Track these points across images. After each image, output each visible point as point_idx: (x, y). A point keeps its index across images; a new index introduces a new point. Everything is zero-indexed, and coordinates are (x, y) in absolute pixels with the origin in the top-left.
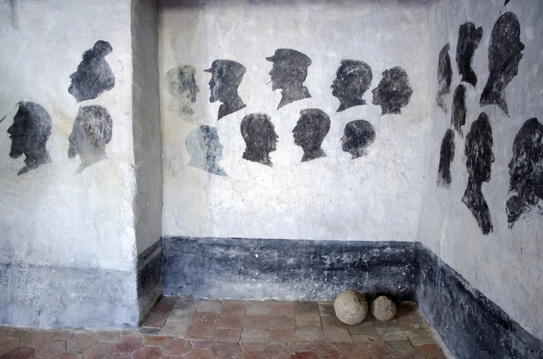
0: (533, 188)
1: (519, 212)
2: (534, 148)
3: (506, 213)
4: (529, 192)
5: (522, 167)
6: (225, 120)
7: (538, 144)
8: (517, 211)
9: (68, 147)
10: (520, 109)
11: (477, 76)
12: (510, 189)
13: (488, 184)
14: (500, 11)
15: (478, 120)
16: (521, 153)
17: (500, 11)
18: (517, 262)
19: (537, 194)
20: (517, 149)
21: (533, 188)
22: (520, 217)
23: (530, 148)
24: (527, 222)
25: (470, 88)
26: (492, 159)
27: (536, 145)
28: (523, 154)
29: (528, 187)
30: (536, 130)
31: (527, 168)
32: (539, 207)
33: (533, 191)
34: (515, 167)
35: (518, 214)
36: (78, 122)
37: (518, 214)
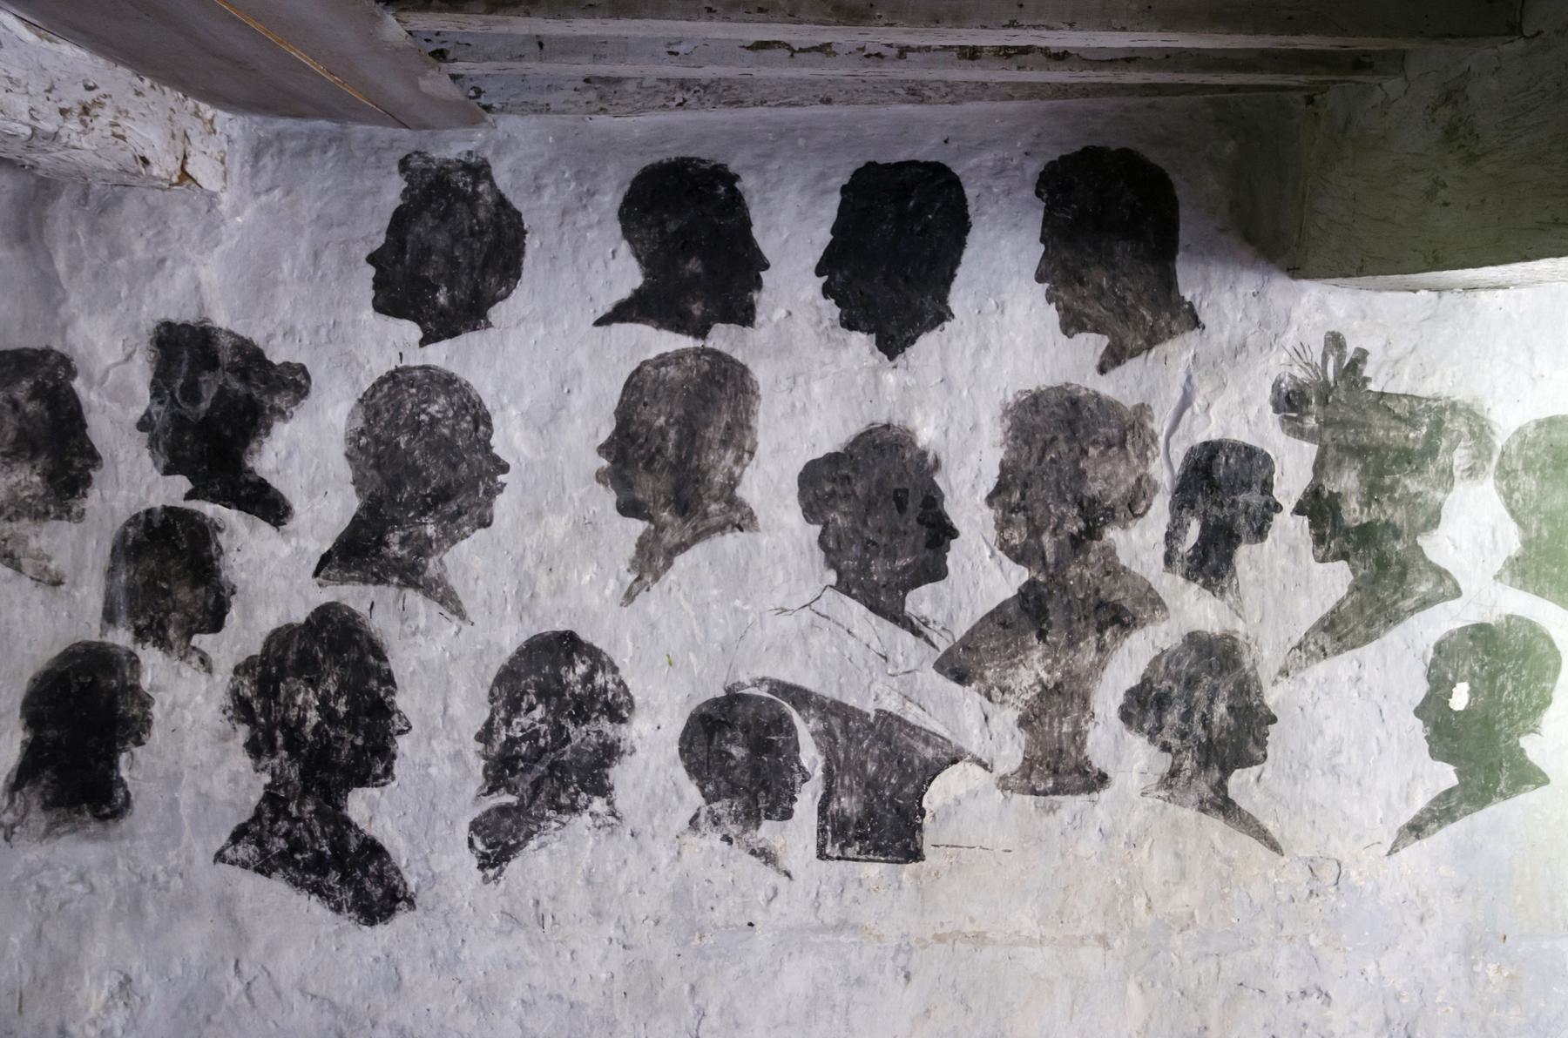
0: (574, 778)
1: (521, 839)
2: (573, 694)
3: (467, 850)
4: (558, 790)
5: (533, 735)
6: (377, 823)
7: (584, 686)
8: (514, 837)
9: (244, 820)
10: (509, 608)
11: (287, 496)
12: (486, 790)
13: (382, 793)
14: (401, 354)
15: (308, 620)
16: (524, 705)
17: (401, 354)
18: (527, 951)
19: (585, 789)
20: (508, 696)
21: (574, 778)
22: (527, 848)
23: (560, 694)
24: (551, 853)
25: (252, 529)
26: (399, 725)
27: (578, 689)
28: (531, 708)
29: (557, 778)
30: (575, 656)
31: (549, 738)
32: (591, 814)
33: (572, 784)
34: (504, 738)
35: (519, 843)
36: (565, 806)
37: (519, 843)
